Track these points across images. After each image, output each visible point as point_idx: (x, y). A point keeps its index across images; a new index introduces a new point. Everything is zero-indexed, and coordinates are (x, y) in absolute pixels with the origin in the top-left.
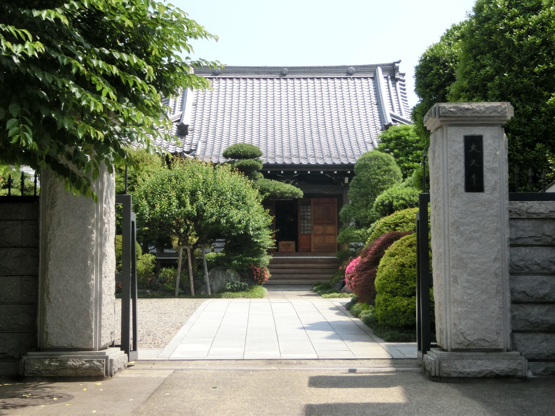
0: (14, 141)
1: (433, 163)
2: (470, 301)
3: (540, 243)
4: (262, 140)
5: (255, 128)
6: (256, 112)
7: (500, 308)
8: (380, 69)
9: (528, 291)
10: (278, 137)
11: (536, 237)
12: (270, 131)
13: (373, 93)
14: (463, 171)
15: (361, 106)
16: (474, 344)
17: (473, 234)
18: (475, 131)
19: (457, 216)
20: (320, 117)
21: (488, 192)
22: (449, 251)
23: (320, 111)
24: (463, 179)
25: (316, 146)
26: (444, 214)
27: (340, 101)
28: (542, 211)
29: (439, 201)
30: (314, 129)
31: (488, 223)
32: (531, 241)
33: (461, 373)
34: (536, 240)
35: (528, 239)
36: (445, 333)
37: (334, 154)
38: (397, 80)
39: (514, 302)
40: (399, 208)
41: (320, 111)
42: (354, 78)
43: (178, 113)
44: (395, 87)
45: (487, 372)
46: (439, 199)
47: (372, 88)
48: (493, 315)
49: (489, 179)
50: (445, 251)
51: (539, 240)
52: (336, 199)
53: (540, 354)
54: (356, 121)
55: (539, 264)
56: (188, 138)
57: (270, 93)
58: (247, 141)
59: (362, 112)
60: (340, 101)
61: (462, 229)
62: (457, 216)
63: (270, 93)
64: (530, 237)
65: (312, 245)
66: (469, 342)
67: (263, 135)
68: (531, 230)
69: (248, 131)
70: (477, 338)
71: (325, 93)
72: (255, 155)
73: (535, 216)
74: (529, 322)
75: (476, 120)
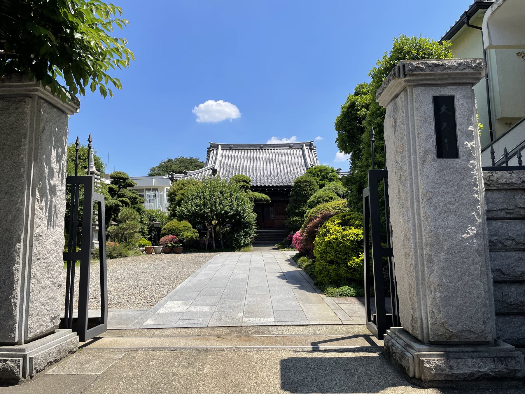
1: (395, 131)
2: (450, 285)
3: (512, 216)
4: (251, 176)
6: (248, 164)
7: (485, 292)
8: (304, 145)
9: (503, 269)
10: (258, 174)
11: (507, 209)
12: (255, 172)
14: (434, 135)
15: (296, 161)
16: (457, 336)
17: (448, 205)
18: (447, 91)
20: (278, 166)
21: (464, 158)
23: (278, 163)
24: (435, 144)
25: (276, 178)
26: (411, 184)
27: (287, 159)
28: (514, 181)
29: (405, 171)
30: (275, 171)
31: (465, 193)
32: (502, 214)
33: (447, 375)
34: (507, 213)
35: (499, 212)
36: (419, 321)
37: (285, 181)
38: (312, 149)
39: (496, 282)
41: (278, 163)
43: (213, 164)
45: (480, 374)
46: (405, 168)
47: (301, 152)
48: (479, 301)
50: (415, 226)
51: (510, 213)
53: (520, 340)
55: (513, 239)
56: (216, 176)
57: (255, 156)
58: (244, 174)
60: (287, 159)
61: (434, 200)
63: (255, 156)
64: (502, 210)
66: (451, 334)
67: (251, 173)
68: (503, 202)
70: (460, 329)
71: (280, 156)
73: (506, 187)
74: (507, 303)
75: (446, 79)
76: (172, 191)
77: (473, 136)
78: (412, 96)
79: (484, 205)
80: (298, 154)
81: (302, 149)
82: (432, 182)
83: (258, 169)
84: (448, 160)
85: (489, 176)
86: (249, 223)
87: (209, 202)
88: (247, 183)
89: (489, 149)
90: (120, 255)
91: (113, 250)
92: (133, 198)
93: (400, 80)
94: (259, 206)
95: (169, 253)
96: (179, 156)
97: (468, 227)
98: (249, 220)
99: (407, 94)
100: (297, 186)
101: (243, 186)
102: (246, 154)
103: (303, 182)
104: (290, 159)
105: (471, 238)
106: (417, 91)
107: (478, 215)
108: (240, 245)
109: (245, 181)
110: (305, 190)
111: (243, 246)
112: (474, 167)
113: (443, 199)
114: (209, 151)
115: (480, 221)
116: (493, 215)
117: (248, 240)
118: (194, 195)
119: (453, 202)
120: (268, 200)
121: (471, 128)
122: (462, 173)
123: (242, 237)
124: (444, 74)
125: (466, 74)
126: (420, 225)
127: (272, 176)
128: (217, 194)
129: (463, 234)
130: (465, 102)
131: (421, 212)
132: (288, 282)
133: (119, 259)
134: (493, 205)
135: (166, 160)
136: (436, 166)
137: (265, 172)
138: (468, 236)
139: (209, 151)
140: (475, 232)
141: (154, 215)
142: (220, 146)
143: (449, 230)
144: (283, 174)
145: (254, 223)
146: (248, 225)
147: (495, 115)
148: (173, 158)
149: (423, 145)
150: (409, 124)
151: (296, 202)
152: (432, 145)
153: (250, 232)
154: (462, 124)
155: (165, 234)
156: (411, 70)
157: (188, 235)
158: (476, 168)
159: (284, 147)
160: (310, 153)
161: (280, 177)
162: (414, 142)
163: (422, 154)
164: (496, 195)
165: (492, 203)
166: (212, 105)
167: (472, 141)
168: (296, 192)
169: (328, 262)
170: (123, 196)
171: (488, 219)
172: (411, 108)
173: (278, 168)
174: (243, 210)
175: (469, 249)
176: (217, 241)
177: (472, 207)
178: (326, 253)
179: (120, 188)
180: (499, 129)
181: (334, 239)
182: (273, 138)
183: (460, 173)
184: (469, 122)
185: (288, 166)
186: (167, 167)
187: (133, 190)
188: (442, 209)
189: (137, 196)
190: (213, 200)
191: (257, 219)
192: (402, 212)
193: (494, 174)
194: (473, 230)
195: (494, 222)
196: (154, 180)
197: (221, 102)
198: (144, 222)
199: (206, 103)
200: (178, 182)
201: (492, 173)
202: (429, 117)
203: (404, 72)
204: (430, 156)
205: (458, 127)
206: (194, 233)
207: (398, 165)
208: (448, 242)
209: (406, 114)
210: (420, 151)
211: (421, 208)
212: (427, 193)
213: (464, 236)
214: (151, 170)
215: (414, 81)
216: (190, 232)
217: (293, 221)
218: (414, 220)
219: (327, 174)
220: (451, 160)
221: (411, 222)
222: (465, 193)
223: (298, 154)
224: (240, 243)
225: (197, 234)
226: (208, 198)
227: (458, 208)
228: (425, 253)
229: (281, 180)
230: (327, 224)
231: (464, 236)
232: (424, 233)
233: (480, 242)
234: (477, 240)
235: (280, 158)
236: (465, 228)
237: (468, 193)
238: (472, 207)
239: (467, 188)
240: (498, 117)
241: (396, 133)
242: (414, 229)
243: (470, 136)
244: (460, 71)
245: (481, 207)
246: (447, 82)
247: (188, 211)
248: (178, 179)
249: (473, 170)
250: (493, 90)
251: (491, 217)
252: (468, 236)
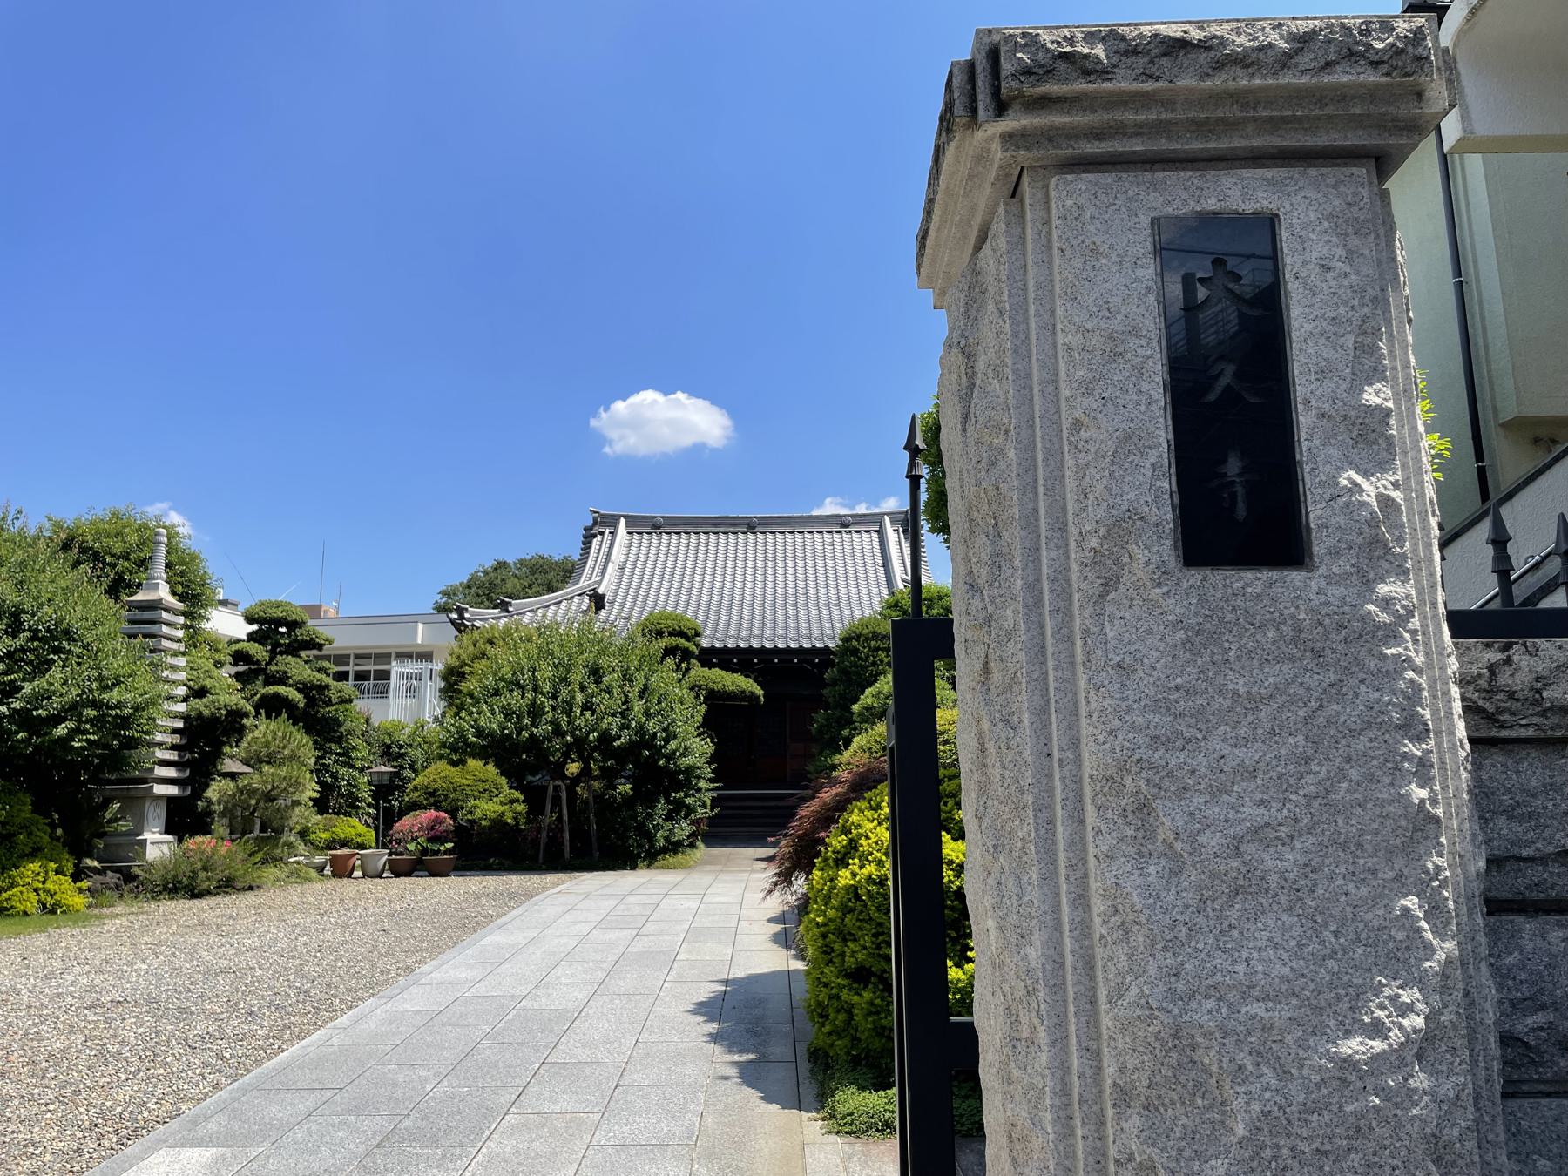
1: (966, 418)
5: (704, 599)
6: (708, 578)
8: (887, 519)
10: (735, 611)
12: (725, 603)
13: (878, 551)
14: (1163, 435)
15: (860, 569)
17: (1251, 849)
18: (1239, 192)
19: (1134, 728)
20: (800, 584)
22: (1090, 967)
23: (800, 576)
24: (1167, 484)
26: (1042, 712)
27: (830, 563)
30: (790, 600)
31: (1354, 774)
40: (555, 584)
49: (1343, 486)
54: (853, 589)
56: (603, 614)
58: (690, 615)
59: (861, 576)
60: (830, 563)
61: (1169, 819)
62: (1134, 728)
69: (693, 602)
71: (809, 552)
72: (693, 635)
75: (1230, 125)
76: (454, 662)
77: (1390, 440)
78: (1047, 222)
79: (1465, 847)
80: (867, 548)
82: (1156, 707)
83: (737, 594)
84: (1248, 575)
85: (1492, 668)
86: (689, 770)
87: (548, 702)
88: (688, 639)
89: (1484, 530)
90: (228, 885)
91: (205, 869)
92: (313, 687)
93: (980, 135)
94: (721, 714)
95: (408, 874)
96: (527, 554)
97: (1377, 990)
98: (685, 762)
99: (1022, 215)
100: (847, 649)
101: (669, 651)
103: (867, 639)
104: (839, 563)
105: (1395, 1060)
106: (1070, 194)
107: (1435, 910)
108: (652, 846)
109: (682, 634)
110: (874, 664)
111: (665, 851)
112: (1403, 620)
113: (1216, 812)
114: (588, 538)
115: (1446, 948)
116: (1521, 884)
117: (683, 829)
118: (502, 679)
119: (1283, 831)
120: (753, 697)
121: (1375, 395)
122: (1330, 657)
123: (661, 821)
124: (1216, 98)
125: (1342, 95)
126: (1089, 966)
127: (780, 616)
128: (577, 675)
129: (1348, 1034)
130: (1340, 252)
131: (1094, 885)
132: (714, 1038)
133: (218, 900)
134: (1518, 828)
135: (489, 564)
136: (1175, 608)
137: (758, 602)
138: (1378, 1045)
139: (588, 538)
140: (1420, 1022)
141: (403, 736)
142: (623, 521)
143: (1258, 1009)
144: (813, 608)
145: (708, 771)
147: (1495, 409)
148: (511, 559)
149: (1099, 488)
150: (1029, 376)
152: (1150, 484)
153: (689, 800)
154: (1322, 374)
155: (415, 806)
156: (1027, 72)
157: (487, 809)
158: (1415, 623)
159: (827, 524)
161: (803, 624)
162: (1057, 475)
163: (1094, 542)
164: (1532, 771)
165: (1511, 818)
166: (655, 401)
167: (1384, 466)
168: (843, 671)
169: (847, 976)
170: (282, 679)
171: (1495, 906)
172: (1039, 287)
173: (800, 591)
174: (665, 730)
175: (1382, 1131)
176: (578, 833)
177: (1399, 863)
178: (845, 936)
179: (273, 654)
180: (1509, 460)
181: (869, 879)
182: (828, 500)
183: (1318, 654)
184: (1368, 363)
185: (831, 583)
186: (492, 587)
187: (318, 658)
188: (1214, 876)
189: (329, 680)
190: (563, 695)
191: (713, 759)
192: (996, 869)
193: (1517, 654)
194: (1406, 1012)
195: (1528, 927)
196: (420, 626)
197: (680, 395)
198: (359, 764)
199: (635, 399)
200: (476, 634)
201: (1507, 647)
202: (1135, 332)
203: (996, 92)
204: (1141, 554)
205: (1304, 386)
206: (512, 801)
207: (976, 602)
208: (1255, 1087)
209: (1014, 323)
210: (1085, 525)
211: (1092, 861)
212: (1123, 769)
213: (1353, 1046)
214: (445, 593)
215: (1050, 137)
216: (495, 800)
218: (1058, 926)
220: (1266, 575)
221: (1037, 938)
222: (1354, 774)
223: (867, 548)
224: (651, 838)
225: (521, 808)
226: (547, 688)
227: (1309, 869)
228: (1113, 1152)
229: (804, 631)
230: (854, 818)
231: (1353, 1046)
232: (1106, 1023)
233: (1448, 1088)
234: (1434, 1073)
235: (809, 559)
236: (1357, 1000)
237: (1371, 778)
238: (1399, 863)
239: (1362, 744)
240: (1505, 416)
241: (970, 429)
242: (1058, 988)
243: (1371, 439)
244: (1304, 80)
245: (1452, 861)
246: (1238, 143)
247: (479, 733)
248: (477, 624)
249: (1392, 636)
250: (1483, 319)
251: (1505, 902)
252: (1378, 1045)
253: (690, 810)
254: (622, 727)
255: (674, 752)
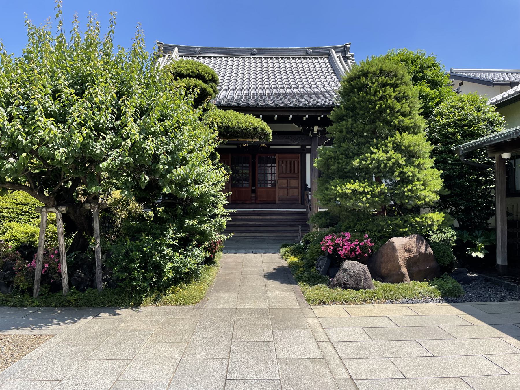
0: (223, 188)
27: (302, 72)
38: (348, 58)
42: (311, 58)
44: (347, 63)
52: (299, 155)
58: (211, 67)
65: (277, 197)
81: (330, 58)
98: (197, 190)
102: (223, 64)
109: (199, 76)
110: (382, 98)
111: (176, 281)
120: (263, 134)
142: (176, 49)
145: (223, 200)
146: (199, 207)
151: (351, 134)
160: (345, 65)
217: (344, 196)
219: (422, 69)
223: (323, 65)
224: (159, 269)
253: (205, 236)
254: (114, 146)
255: (184, 179)
